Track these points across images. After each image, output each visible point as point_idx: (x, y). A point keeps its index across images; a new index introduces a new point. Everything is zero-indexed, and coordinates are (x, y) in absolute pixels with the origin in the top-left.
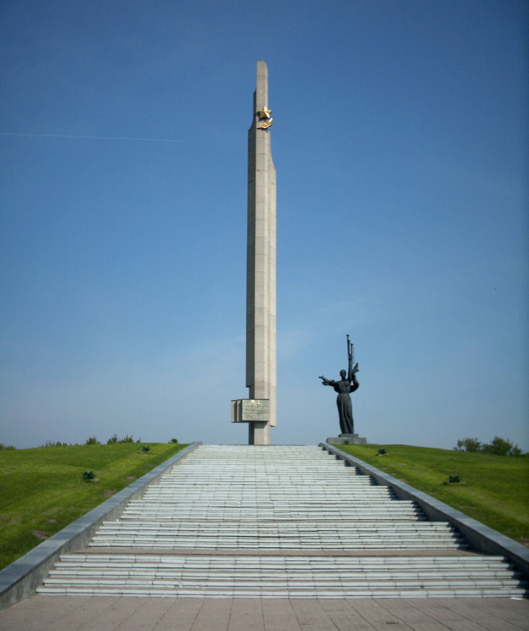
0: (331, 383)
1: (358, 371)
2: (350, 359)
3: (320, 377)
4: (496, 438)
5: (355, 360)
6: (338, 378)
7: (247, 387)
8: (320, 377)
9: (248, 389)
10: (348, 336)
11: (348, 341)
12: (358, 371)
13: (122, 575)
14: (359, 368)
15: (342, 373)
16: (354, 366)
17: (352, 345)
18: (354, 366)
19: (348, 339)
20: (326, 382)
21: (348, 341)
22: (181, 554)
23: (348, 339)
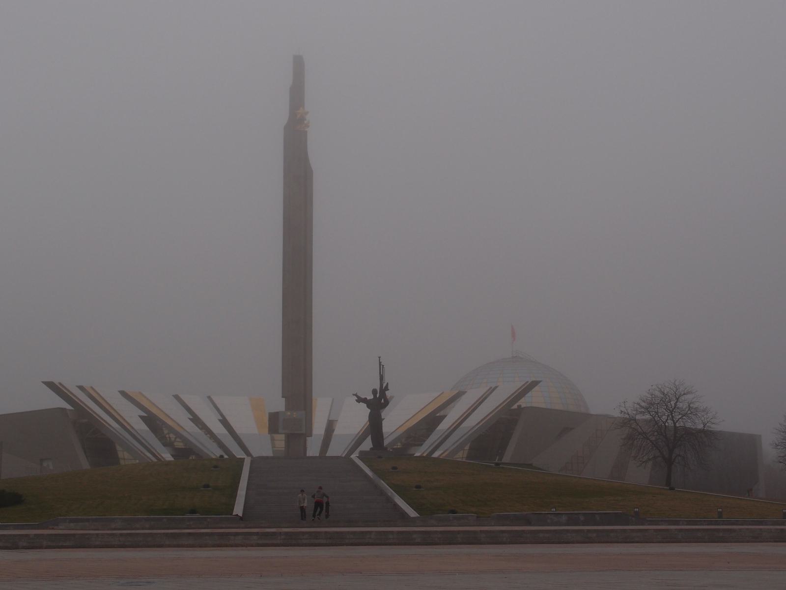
0: (364, 401)
1: (388, 390)
2: (382, 378)
3: (354, 395)
4: (760, 436)
5: (387, 379)
6: (370, 397)
7: (283, 397)
8: (354, 395)
9: (284, 399)
10: (380, 357)
11: (380, 363)
12: (388, 390)
13: (141, 582)
14: (389, 387)
15: (374, 392)
16: (384, 385)
17: (383, 366)
18: (384, 385)
19: (380, 360)
20: (360, 400)
21: (380, 363)
22: (486, 398)
23: (380, 360)
